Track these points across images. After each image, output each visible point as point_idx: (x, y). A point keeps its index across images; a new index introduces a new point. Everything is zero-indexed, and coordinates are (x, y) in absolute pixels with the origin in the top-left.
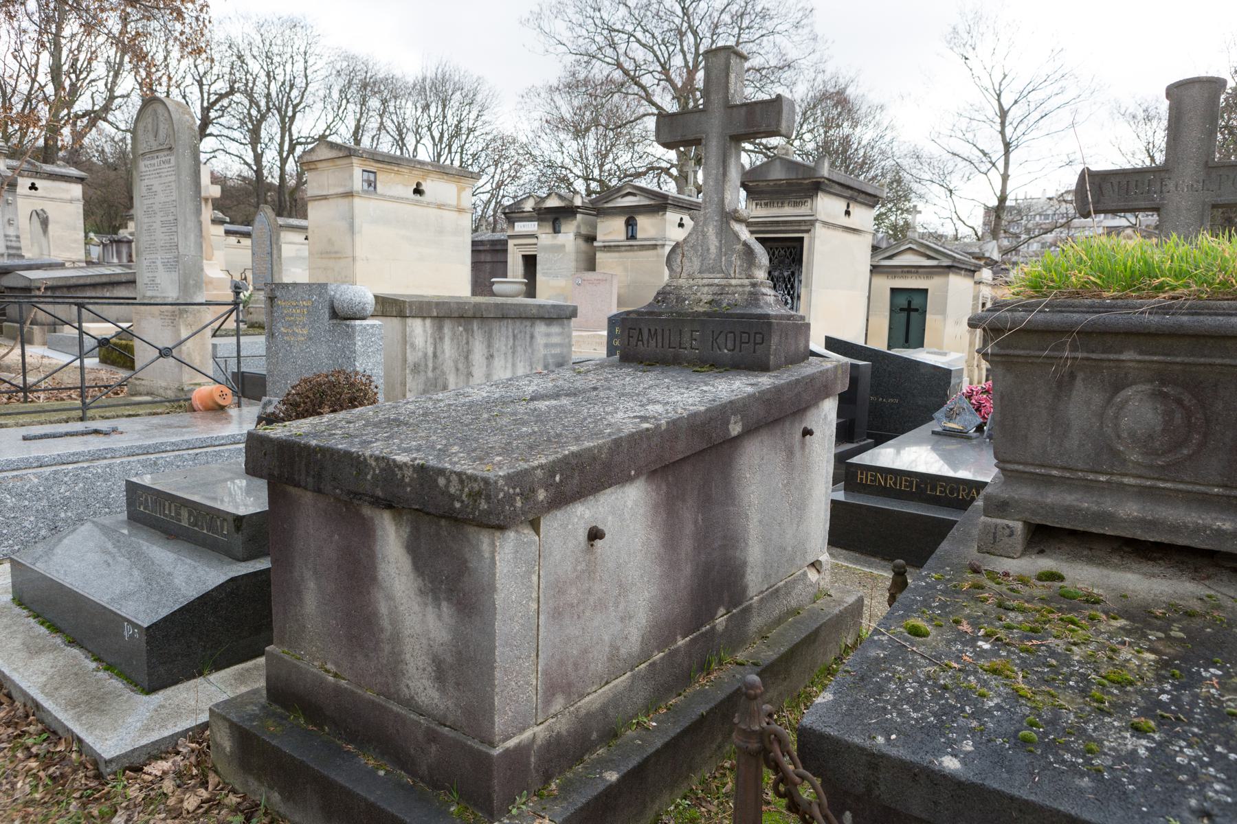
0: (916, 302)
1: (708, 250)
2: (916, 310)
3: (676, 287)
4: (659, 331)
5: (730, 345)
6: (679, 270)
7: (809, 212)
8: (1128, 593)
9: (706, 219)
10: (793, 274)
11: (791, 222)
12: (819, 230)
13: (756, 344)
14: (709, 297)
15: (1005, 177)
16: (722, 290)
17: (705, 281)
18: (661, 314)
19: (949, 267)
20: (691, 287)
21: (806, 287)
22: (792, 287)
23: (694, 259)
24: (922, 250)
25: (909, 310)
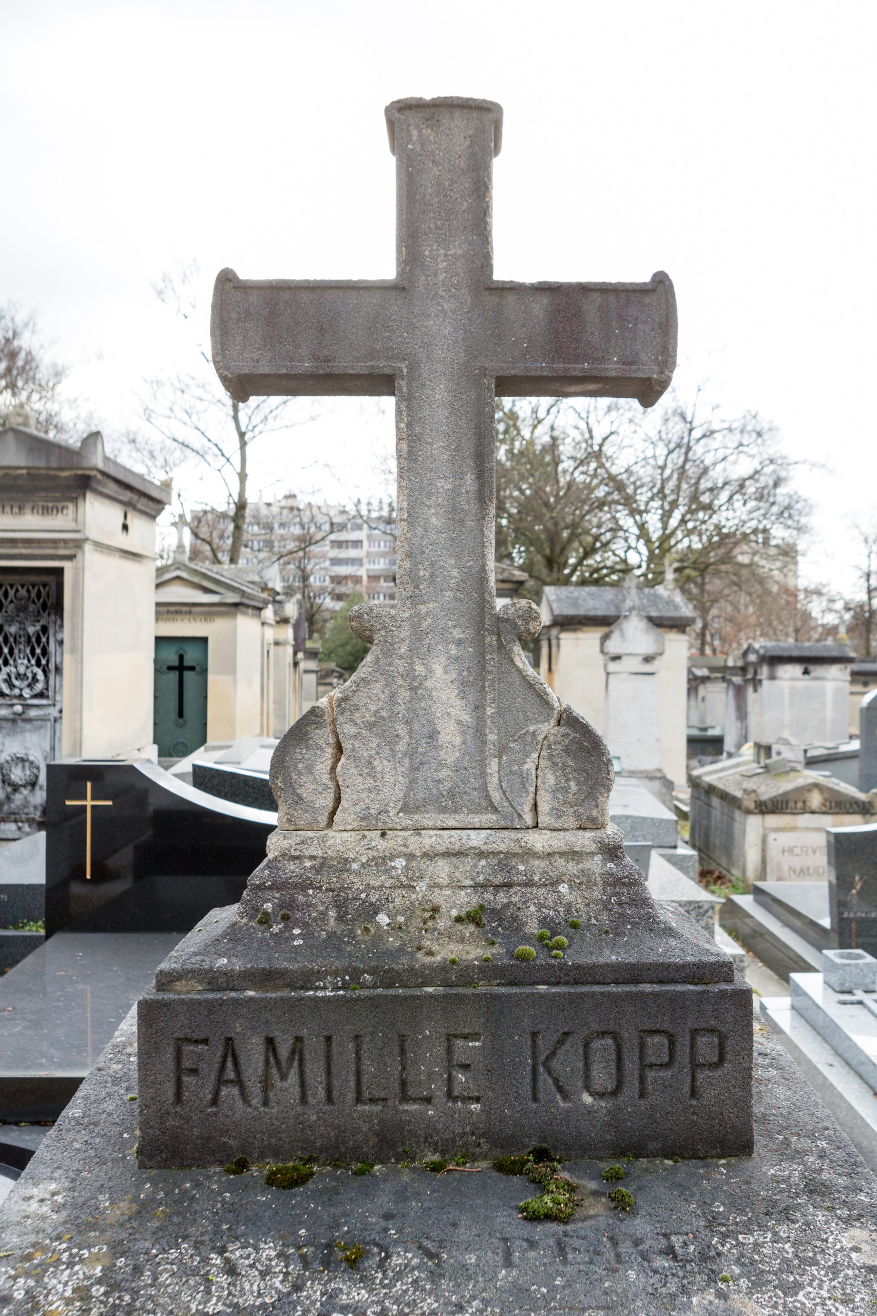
0: (191, 656)
1: (433, 735)
2: (192, 668)
3: (323, 865)
4: (314, 1047)
5: (602, 1077)
6: (326, 801)
7: (72, 525)
9: (418, 635)
10: (45, 629)
11: (39, 541)
12: (90, 556)
13: (695, 1066)
14: (466, 900)
15: (243, 476)
17: (429, 840)
18: (307, 980)
19: (236, 605)
20: (381, 862)
21: (73, 651)
22: (45, 652)
24: (196, 579)
25: (181, 668)
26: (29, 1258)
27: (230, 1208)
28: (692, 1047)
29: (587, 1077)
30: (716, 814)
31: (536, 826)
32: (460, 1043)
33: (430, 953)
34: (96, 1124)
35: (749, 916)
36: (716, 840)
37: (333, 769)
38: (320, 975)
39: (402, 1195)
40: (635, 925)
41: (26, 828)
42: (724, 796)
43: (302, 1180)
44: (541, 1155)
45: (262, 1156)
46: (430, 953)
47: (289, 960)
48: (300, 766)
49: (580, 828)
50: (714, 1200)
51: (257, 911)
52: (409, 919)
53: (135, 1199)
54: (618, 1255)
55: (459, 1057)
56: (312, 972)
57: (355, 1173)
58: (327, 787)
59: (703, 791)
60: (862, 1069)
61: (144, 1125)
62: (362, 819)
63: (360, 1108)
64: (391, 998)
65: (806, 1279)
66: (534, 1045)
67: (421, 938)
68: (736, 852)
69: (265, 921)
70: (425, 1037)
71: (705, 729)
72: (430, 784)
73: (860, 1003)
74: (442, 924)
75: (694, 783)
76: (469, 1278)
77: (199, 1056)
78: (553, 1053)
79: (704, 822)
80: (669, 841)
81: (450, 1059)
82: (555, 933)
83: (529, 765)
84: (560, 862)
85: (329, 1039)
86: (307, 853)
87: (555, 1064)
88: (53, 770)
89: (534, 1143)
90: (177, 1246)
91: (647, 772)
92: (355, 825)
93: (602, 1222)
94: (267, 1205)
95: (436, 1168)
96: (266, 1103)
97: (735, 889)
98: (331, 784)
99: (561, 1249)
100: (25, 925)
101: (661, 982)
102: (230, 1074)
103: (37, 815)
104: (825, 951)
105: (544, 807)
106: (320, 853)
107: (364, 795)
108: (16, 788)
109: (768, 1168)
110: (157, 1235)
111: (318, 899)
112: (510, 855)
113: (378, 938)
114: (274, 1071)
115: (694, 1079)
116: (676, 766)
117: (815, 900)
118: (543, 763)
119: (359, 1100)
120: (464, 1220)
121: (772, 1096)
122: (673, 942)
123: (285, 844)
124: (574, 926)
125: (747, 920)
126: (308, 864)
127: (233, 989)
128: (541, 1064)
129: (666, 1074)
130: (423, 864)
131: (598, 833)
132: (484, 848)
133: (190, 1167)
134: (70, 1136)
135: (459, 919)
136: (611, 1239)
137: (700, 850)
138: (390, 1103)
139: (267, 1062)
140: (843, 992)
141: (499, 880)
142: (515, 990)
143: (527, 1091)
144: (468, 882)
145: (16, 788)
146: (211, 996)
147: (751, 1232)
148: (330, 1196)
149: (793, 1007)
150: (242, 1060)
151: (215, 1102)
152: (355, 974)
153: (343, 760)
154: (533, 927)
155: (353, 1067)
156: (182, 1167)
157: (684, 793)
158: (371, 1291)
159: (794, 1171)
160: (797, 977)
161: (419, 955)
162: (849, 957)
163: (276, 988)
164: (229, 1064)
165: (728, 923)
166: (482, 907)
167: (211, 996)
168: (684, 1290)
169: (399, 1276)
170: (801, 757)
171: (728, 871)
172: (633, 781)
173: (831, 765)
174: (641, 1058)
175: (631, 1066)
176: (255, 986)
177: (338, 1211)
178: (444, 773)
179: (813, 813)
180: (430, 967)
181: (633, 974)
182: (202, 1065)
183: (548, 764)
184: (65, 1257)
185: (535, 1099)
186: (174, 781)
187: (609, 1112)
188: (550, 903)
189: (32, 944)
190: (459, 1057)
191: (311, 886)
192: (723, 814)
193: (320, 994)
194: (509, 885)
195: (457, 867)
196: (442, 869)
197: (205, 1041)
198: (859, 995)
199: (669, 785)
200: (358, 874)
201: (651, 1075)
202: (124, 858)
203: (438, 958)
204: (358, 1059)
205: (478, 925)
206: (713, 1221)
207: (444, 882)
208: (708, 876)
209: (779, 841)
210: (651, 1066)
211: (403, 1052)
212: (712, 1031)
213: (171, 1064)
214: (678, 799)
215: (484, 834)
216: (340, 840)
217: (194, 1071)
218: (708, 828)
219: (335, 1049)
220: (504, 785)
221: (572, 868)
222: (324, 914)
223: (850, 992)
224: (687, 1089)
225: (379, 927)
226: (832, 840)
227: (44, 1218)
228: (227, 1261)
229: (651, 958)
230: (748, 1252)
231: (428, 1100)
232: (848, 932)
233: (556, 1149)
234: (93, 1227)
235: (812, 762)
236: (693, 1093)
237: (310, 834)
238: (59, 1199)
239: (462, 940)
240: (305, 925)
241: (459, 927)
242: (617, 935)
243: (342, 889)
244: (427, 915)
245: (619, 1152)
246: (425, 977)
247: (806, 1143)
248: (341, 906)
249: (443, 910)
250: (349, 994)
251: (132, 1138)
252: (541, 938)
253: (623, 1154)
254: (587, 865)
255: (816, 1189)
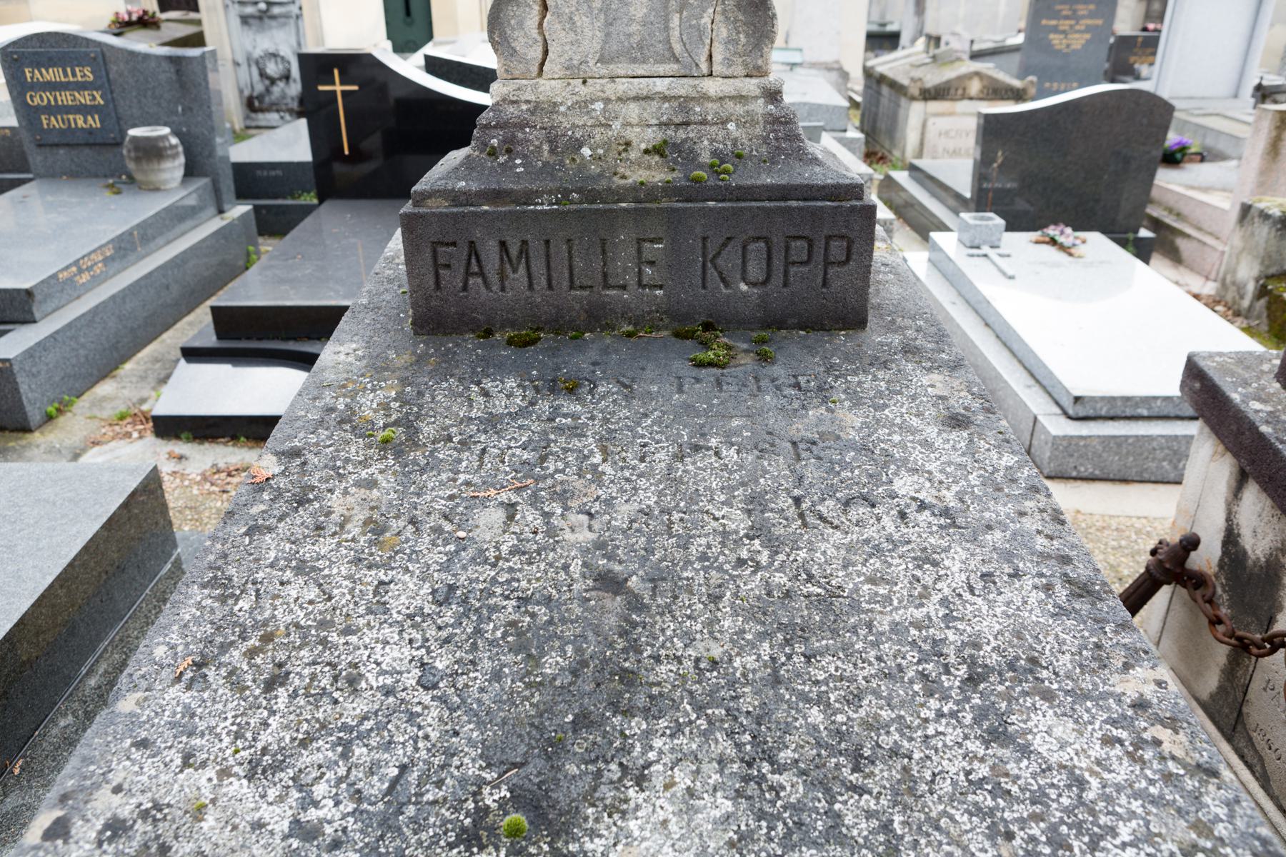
3: (536, 108)
4: (536, 248)
5: (755, 271)
6: (537, 53)
8: (107, 193)
13: (827, 264)
14: (652, 136)
16: (683, 112)
17: (622, 86)
18: (529, 197)
20: (583, 105)
23: (582, 21)
26: (344, 386)
27: (482, 359)
28: (826, 249)
29: (744, 271)
30: (884, 101)
31: (711, 75)
32: (647, 245)
33: (624, 177)
34: (379, 308)
35: (903, 189)
36: (882, 125)
37: (540, 25)
38: (538, 194)
39: (605, 351)
40: (788, 156)
41: (288, 117)
42: (894, 85)
43: (533, 342)
44: (708, 327)
45: (503, 327)
46: (624, 177)
47: (513, 183)
48: (513, 22)
49: (747, 76)
50: (833, 356)
51: (486, 145)
52: (607, 151)
53: (414, 353)
54: (759, 388)
55: (647, 255)
56: (532, 192)
57: (571, 338)
58: (536, 41)
59: (875, 80)
60: (978, 307)
61: (415, 305)
62: (567, 69)
63: (573, 293)
64: (596, 210)
65: (892, 402)
66: (704, 246)
67: (617, 166)
68: (898, 135)
69: (493, 153)
70: (621, 241)
71: (884, 25)
72: (622, 37)
73: (985, 256)
74: (633, 155)
75: (868, 73)
76: (652, 399)
77: (450, 254)
78: (719, 253)
79: (873, 109)
80: (841, 125)
81: (640, 257)
82: (723, 162)
83: (706, 20)
84: (730, 105)
85: (547, 242)
86: (523, 99)
87: (720, 261)
88: (304, 59)
89: (703, 319)
90: (447, 381)
91: (826, 63)
92: (561, 74)
93: (749, 368)
94: (508, 357)
95: (630, 335)
96: (503, 289)
97: (895, 167)
98: (539, 38)
99: (719, 383)
100: (300, 196)
101: (805, 199)
102: (475, 269)
103: (295, 105)
104: (962, 215)
105: (717, 58)
106: (533, 98)
107: (567, 48)
108: (273, 81)
109: (876, 336)
110: (432, 374)
111: (534, 135)
112: (688, 99)
113: (584, 165)
114: (508, 266)
115: (826, 273)
116: (854, 58)
117: (961, 176)
118: (718, 18)
119: (572, 287)
120: (650, 366)
121: (884, 290)
122: (817, 169)
123: (505, 90)
124: (739, 156)
125: (902, 194)
126: (524, 107)
127: (471, 205)
128: (710, 260)
129: (805, 269)
130: (618, 107)
131: (762, 80)
132: (667, 93)
133: (451, 334)
134: (361, 316)
135: (646, 152)
136: (755, 378)
137: (867, 134)
138: (595, 289)
139: (502, 259)
140: (972, 247)
141: (679, 119)
142: (690, 205)
143: (698, 281)
144: (654, 121)
145: (273, 81)
146: (455, 210)
147: (857, 375)
148: (554, 352)
149: (929, 260)
150: (483, 257)
151: (465, 288)
152: (566, 193)
153: (548, 16)
154: (705, 158)
155: (566, 263)
156: (445, 334)
157: (857, 84)
158: (583, 406)
159: (896, 340)
160: (935, 236)
161: (616, 179)
162: (982, 219)
163: (505, 204)
164: (473, 261)
165: (885, 196)
166: (665, 142)
167: (455, 210)
168: (804, 407)
169: (603, 397)
170: (966, 47)
171: (890, 152)
172: (813, 72)
173: (997, 58)
174: (786, 257)
175: (778, 263)
176: (488, 202)
177: (560, 360)
178: (634, 28)
179: (971, 99)
180: (624, 187)
181: (784, 193)
182: (453, 261)
183: (722, 18)
184: (369, 386)
185: (704, 287)
186: (411, 68)
187: (760, 297)
188: (720, 138)
189: (307, 210)
190: (647, 255)
191: (527, 125)
192: (890, 100)
193: (539, 208)
194: (687, 124)
195: (645, 109)
196: (633, 111)
197: (454, 244)
198: (985, 249)
199: (845, 76)
200: (565, 115)
201: (793, 270)
202: (373, 142)
203: (630, 181)
204: (570, 257)
205: (662, 155)
206: (830, 369)
207: (635, 120)
208: (872, 156)
209: (936, 125)
210: (794, 263)
211: (604, 252)
212: (842, 237)
213: (430, 261)
214: (853, 91)
215: (667, 80)
216: (549, 87)
217: (448, 266)
218: (876, 114)
219: (553, 250)
220: (685, 38)
221: (739, 109)
222: (539, 147)
223: (978, 247)
224: (820, 280)
225: (583, 157)
226: (982, 121)
227: (351, 364)
228: (483, 389)
229: (799, 181)
230: (853, 386)
231: (624, 287)
232: (982, 200)
233: (719, 322)
234: (386, 369)
235: (975, 56)
236: (825, 283)
237: (524, 82)
238: (360, 353)
239: (649, 167)
240: (525, 157)
241: (647, 157)
242: (773, 163)
243: (553, 127)
244: (621, 148)
245: (766, 325)
246: (620, 195)
247: (908, 322)
248: (552, 141)
249: (634, 144)
250: (561, 208)
251: (407, 316)
252: (712, 166)
253: (769, 327)
254: (751, 107)
255: (909, 350)
